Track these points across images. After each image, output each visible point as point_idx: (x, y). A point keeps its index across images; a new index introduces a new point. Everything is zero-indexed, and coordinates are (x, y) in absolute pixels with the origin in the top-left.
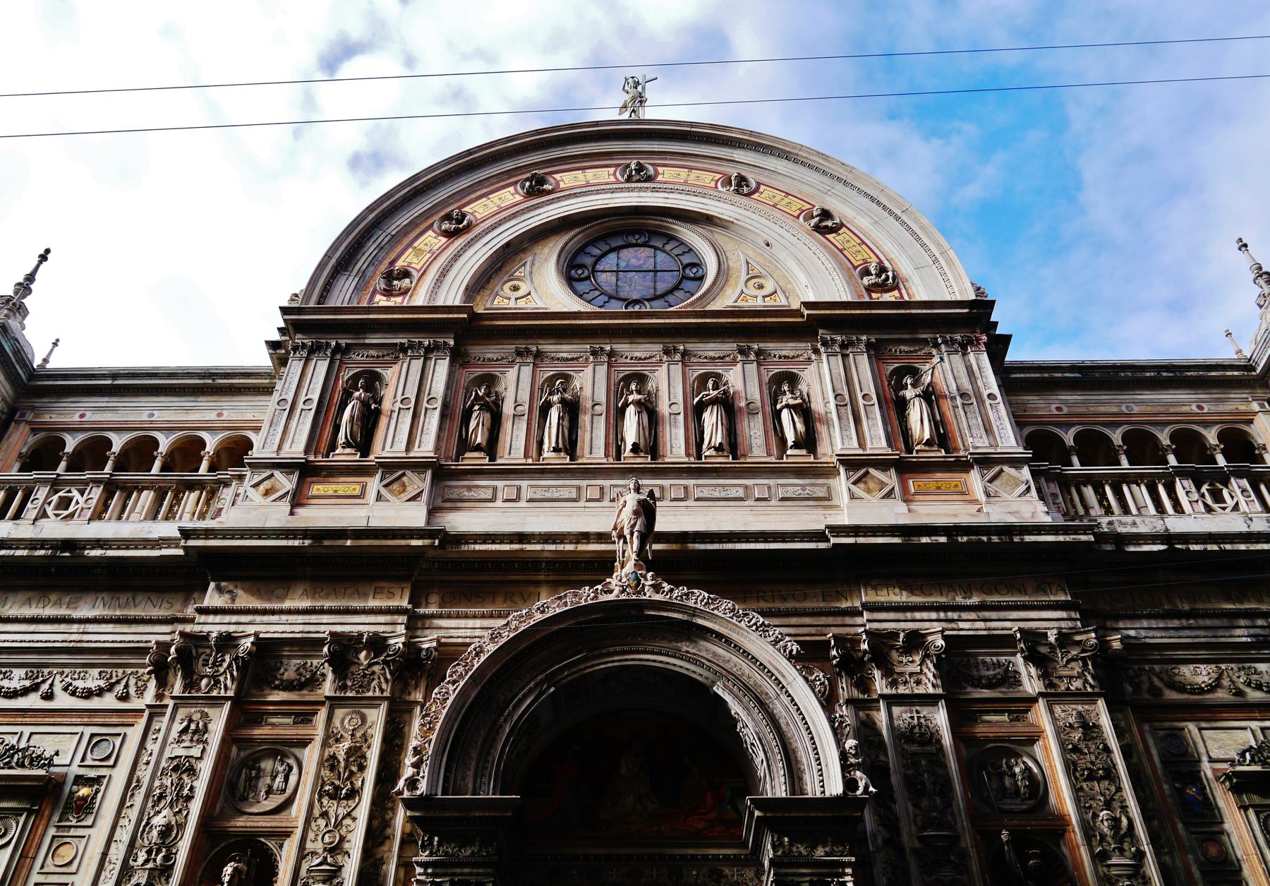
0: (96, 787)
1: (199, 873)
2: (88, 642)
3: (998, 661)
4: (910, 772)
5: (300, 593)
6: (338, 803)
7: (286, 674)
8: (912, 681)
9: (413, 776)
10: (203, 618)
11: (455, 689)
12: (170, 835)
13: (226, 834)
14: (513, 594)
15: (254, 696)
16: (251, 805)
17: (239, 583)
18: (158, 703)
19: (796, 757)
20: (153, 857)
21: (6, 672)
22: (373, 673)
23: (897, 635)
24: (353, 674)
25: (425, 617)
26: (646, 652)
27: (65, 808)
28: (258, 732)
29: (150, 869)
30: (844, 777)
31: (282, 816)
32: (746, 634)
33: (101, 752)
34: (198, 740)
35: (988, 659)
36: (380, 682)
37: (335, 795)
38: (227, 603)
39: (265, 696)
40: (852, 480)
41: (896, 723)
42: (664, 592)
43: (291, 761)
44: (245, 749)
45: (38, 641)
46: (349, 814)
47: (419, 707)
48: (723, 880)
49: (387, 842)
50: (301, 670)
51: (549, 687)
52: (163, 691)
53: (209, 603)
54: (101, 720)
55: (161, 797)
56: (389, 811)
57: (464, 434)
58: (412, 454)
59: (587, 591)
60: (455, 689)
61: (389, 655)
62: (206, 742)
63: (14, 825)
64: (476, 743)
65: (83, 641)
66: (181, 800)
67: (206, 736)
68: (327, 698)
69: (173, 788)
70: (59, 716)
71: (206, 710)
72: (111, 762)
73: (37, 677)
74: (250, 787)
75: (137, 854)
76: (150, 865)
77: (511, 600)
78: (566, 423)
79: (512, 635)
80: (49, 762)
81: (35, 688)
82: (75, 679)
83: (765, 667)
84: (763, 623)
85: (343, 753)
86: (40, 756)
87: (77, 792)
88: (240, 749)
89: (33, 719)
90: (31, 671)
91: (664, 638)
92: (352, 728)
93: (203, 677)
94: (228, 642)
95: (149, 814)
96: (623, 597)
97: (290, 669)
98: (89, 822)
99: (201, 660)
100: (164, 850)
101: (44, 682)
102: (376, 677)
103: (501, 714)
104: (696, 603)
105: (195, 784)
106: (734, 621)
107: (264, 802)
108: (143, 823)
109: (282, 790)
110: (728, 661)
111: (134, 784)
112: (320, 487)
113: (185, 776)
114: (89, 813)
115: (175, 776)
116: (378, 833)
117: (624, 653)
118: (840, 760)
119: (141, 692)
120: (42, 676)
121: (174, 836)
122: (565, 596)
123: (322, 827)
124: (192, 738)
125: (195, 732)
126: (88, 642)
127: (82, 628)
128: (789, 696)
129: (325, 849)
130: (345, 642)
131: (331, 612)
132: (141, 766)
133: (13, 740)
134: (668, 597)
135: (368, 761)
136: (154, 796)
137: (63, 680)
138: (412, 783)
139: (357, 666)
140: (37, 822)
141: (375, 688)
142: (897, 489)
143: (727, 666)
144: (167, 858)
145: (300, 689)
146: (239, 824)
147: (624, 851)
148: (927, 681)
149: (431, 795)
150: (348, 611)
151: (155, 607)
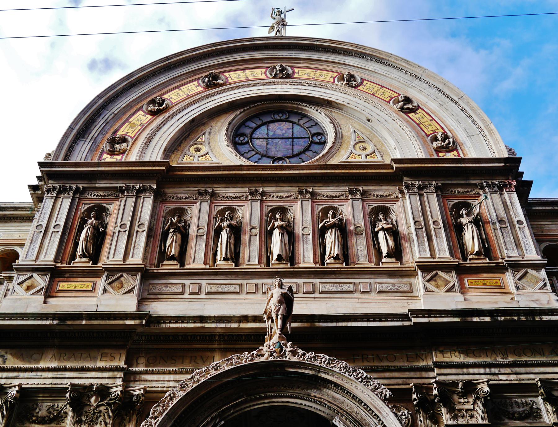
3: (526, 401)
5: (50, 357)
7: (40, 413)
8: (468, 415)
11: (156, 423)
17: (8, 350)
22: (100, 412)
23: (458, 384)
24: (86, 412)
25: (136, 373)
32: (355, 384)
35: (519, 400)
36: (105, 418)
40: (427, 279)
42: (299, 355)
50: (51, 410)
51: (220, 421)
57: (163, 248)
58: (127, 262)
59: (246, 355)
60: (156, 423)
61: (111, 400)
78: (232, 241)
79: (195, 385)
83: (368, 407)
84: (366, 376)
91: (299, 387)
96: (271, 359)
102: (102, 414)
104: (321, 363)
106: (347, 375)
110: (343, 403)
112: (64, 284)
130: (81, 391)
131: (71, 370)
134: (302, 359)
139: (89, 407)
141: (101, 422)
142: (456, 285)
143: (342, 406)
148: (478, 415)
150: (83, 369)
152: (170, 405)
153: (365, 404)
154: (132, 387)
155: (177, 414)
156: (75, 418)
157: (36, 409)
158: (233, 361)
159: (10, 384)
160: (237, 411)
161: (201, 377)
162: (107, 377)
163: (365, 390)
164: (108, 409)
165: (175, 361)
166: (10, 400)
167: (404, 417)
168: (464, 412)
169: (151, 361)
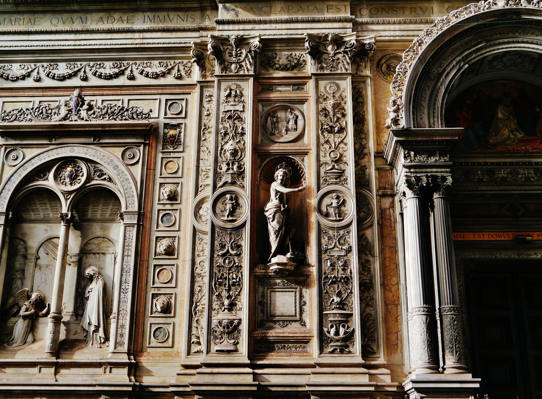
0: (178, 130)
1: (258, 176)
2: (148, 44)
5: (279, 9)
6: (334, 135)
7: (281, 61)
9: (396, 117)
10: (221, 27)
11: (410, 66)
12: (237, 155)
13: (268, 154)
14: (416, 9)
15: (264, 74)
16: (279, 138)
17: (238, 4)
18: (204, 80)
20: (231, 166)
21: (100, 64)
22: (338, 59)
24: (326, 60)
25: (362, 24)
26: (523, 42)
27: (163, 142)
28: (273, 96)
29: (231, 173)
31: (299, 143)
33: (176, 109)
34: (238, 101)
36: (344, 65)
37: (331, 131)
38: (233, 17)
39: (271, 74)
42: (533, 3)
43: (297, 113)
44: (267, 106)
45: (116, 44)
46: (342, 141)
47: (369, 79)
49: (366, 156)
50: (290, 58)
51: (464, 65)
52: (205, 72)
53: (222, 17)
54: (169, 91)
55: (226, 134)
56: (364, 140)
60: (410, 66)
61: (346, 48)
62: (243, 102)
63: (138, 152)
64: (425, 98)
65: (144, 44)
66: (238, 135)
67: (243, 98)
68: (313, 74)
69: (232, 129)
70: (143, 89)
71: (238, 83)
72: (183, 115)
73: (121, 67)
74: (275, 128)
75: (220, 166)
76: (231, 171)
77: (415, 12)
79: (440, 32)
80: (148, 116)
81: (122, 73)
82: (145, 67)
85: (330, 107)
86: (141, 112)
87: (168, 133)
88: (263, 106)
89: (127, 92)
90: (115, 63)
91: (533, 34)
92: (332, 92)
93: (231, 63)
94: (241, 42)
95: (221, 144)
97: (283, 57)
98: (181, 150)
99: (227, 53)
100: (236, 163)
101: (126, 69)
102: (340, 61)
103: (438, 81)
105: (244, 126)
107: (286, 136)
108: (219, 149)
109: (295, 129)
111: (203, 128)
113: (236, 122)
114: (179, 144)
115: (231, 122)
116: (360, 152)
117: (509, 43)
119: (189, 73)
120: (124, 66)
121: (240, 155)
122: (470, 7)
123: (328, 149)
124: (234, 99)
125: (236, 96)
126: (148, 44)
127: (141, 35)
129: (332, 161)
130: (317, 40)
131: (303, 21)
132: (205, 118)
133: (120, 103)
134: (537, 6)
135: (347, 111)
136: (221, 133)
137: (138, 68)
138: (396, 121)
139: (327, 55)
140: (150, 150)
141: (341, 68)
144: (240, 167)
145: (292, 70)
146: (275, 148)
147: (508, 160)
149: (408, 128)
150: (313, 21)
151: (183, 21)
152: (420, 50)
154: (360, 36)
155: (427, 58)
156: (317, 64)
157: (276, 57)
158: (472, 9)
159: (248, 35)
160: (478, 56)
161: (444, 24)
162: (337, 27)
164: (345, 57)
165: (396, 13)
166: (254, 49)
169: (373, 13)
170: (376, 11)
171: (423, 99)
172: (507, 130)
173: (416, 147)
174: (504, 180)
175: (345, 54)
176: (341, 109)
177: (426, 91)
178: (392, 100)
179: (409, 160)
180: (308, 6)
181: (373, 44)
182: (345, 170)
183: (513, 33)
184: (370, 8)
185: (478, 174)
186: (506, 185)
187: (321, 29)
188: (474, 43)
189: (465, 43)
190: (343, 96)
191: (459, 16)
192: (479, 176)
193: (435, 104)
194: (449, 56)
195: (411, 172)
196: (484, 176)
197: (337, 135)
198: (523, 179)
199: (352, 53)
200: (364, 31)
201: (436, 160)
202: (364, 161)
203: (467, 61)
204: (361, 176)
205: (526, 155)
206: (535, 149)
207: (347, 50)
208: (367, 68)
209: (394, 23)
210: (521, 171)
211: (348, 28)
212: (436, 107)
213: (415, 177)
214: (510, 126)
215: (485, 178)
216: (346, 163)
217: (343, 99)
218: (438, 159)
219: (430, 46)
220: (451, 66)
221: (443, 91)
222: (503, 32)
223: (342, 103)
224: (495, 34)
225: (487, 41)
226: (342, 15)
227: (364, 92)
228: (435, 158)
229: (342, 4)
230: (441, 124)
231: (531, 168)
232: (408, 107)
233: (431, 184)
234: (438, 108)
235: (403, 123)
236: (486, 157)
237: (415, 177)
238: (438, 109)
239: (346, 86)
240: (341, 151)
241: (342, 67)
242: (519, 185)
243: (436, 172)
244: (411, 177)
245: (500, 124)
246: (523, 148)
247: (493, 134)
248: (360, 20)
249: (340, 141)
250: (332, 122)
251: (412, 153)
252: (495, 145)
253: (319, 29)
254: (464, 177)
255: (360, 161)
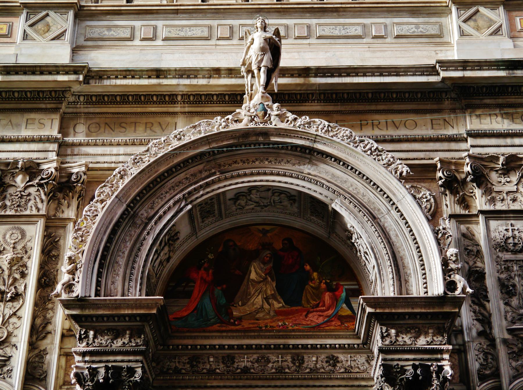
4: (503, 276)
6: (5, 305)
8: (509, 198)
9: (69, 281)
11: (103, 207)
14: (152, 124)
19: (403, 263)
23: (497, 158)
25: (73, 145)
30: (445, 279)
32: (361, 157)
41: (493, 235)
42: (288, 121)
46: (14, 314)
48: (338, 365)
49: (49, 336)
51: (187, 205)
60: (103, 207)
61: (42, 179)
64: (123, 253)
79: (152, 160)
84: (377, 148)
85: (6, 263)
92: (13, 242)
102: (32, 197)
103: (144, 229)
110: (346, 182)
116: (40, 329)
118: (442, 265)
128: (399, 211)
134: (292, 125)
135: (29, 269)
138: (69, 287)
139: (14, 188)
141: (31, 207)
143: (344, 186)
149: (85, 296)
152: (120, 185)
153: (374, 184)
158: (202, 129)
160: (208, 193)
162: (36, 150)
163: (374, 166)
164: (40, 192)
167: (425, 200)
168: (505, 195)
170: (96, 127)
171: (121, 254)
172: (260, 297)
173: (97, 324)
174: (246, 370)
175: (39, 188)
176: (22, 266)
177: (126, 242)
178: (68, 256)
179: (84, 344)
180: (52, 120)
181: (82, 174)
182: (11, 356)
183: (262, 161)
184: (89, 122)
185: (209, 362)
186: (247, 379)
187: (12, 151)
188: (204, 174)
189: (192, 175)
190: (27, 247)
191: (182, 137)
192: (211, 365)
193: (134, 262)
194: (166, 193)
195: (85, 362)
196: (218, 365)
197: (10, 304)
198: (274, 370)
199: (50, 187)
200: (75, 155)
201: (124, 343)
202: (44, 344)
203: (190, 200)
204: (36, 365)
205: (281, 334)
206: (296, 325)
207: (42, 182)
208: (70, 208)
209: (118, 145)
210: (273, 358)
211: (50, 151)
212: (136, 266)
213: (89, 368)
214: (266, 291)
215: (219, 369)
216: (14, 345)
217: (26, 252)
218: (126, 342)
219: (135, 180)
220: (166, 207)
221: (150, 242)
222: (247, 160)
223: (25, 257)
224: (235, 162)
225: (222, 173)
226: (45, 133)
227: (61, 242)
228: (123, 340)
229: (48, 117)
230: (140, 290)
231: (287, 354)
232: (91, 266)
233: (110, 379)
234: (139, 266)
235: (78, 291)
236: (222, 337)
237: (89, 368)
238: (139, 269)
239: (34, 234)
240: (10, 328)
241: (33, 206)
242: (266, 379)
243: (122, 361)
244: (83, 368)
245: (252, 288)
246: (280, 324)
247: (240, 303)
248: (70, 139)
249: (11, 313)
250: (5, 285)
251: (91, 333)
252: (240, 319)
253: (10, 151)
254: (189, 366)
255: (39, 343)
